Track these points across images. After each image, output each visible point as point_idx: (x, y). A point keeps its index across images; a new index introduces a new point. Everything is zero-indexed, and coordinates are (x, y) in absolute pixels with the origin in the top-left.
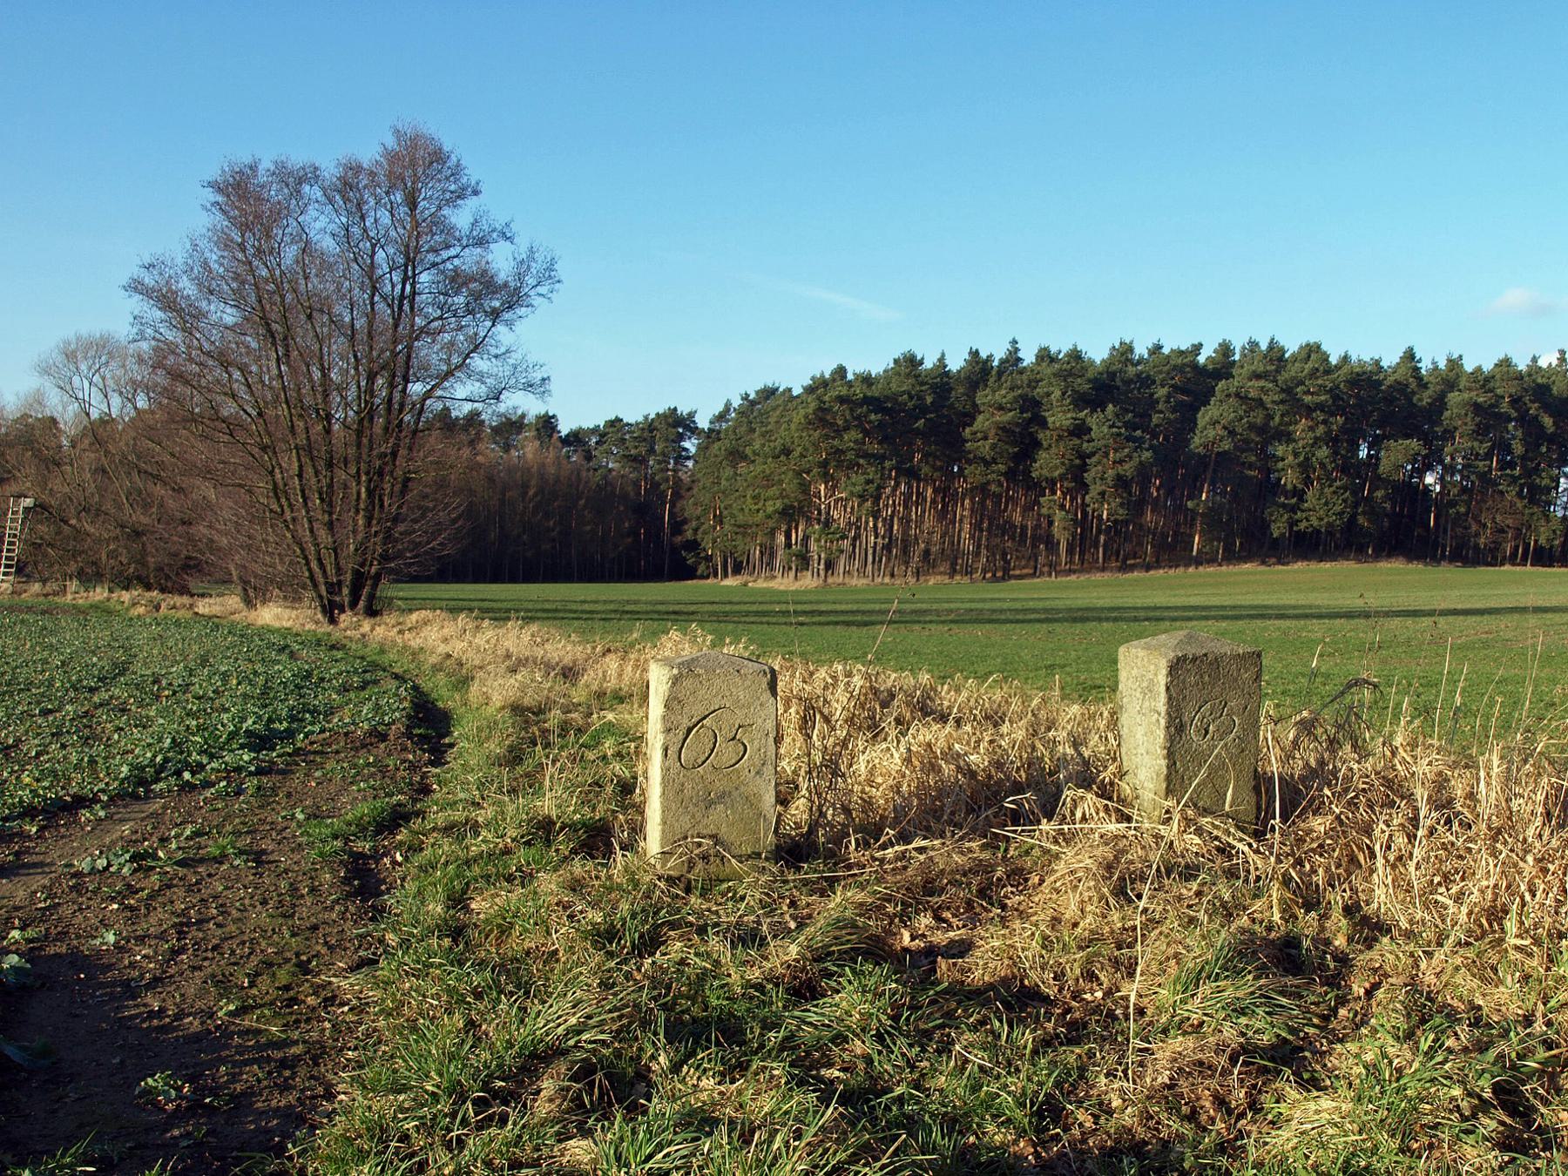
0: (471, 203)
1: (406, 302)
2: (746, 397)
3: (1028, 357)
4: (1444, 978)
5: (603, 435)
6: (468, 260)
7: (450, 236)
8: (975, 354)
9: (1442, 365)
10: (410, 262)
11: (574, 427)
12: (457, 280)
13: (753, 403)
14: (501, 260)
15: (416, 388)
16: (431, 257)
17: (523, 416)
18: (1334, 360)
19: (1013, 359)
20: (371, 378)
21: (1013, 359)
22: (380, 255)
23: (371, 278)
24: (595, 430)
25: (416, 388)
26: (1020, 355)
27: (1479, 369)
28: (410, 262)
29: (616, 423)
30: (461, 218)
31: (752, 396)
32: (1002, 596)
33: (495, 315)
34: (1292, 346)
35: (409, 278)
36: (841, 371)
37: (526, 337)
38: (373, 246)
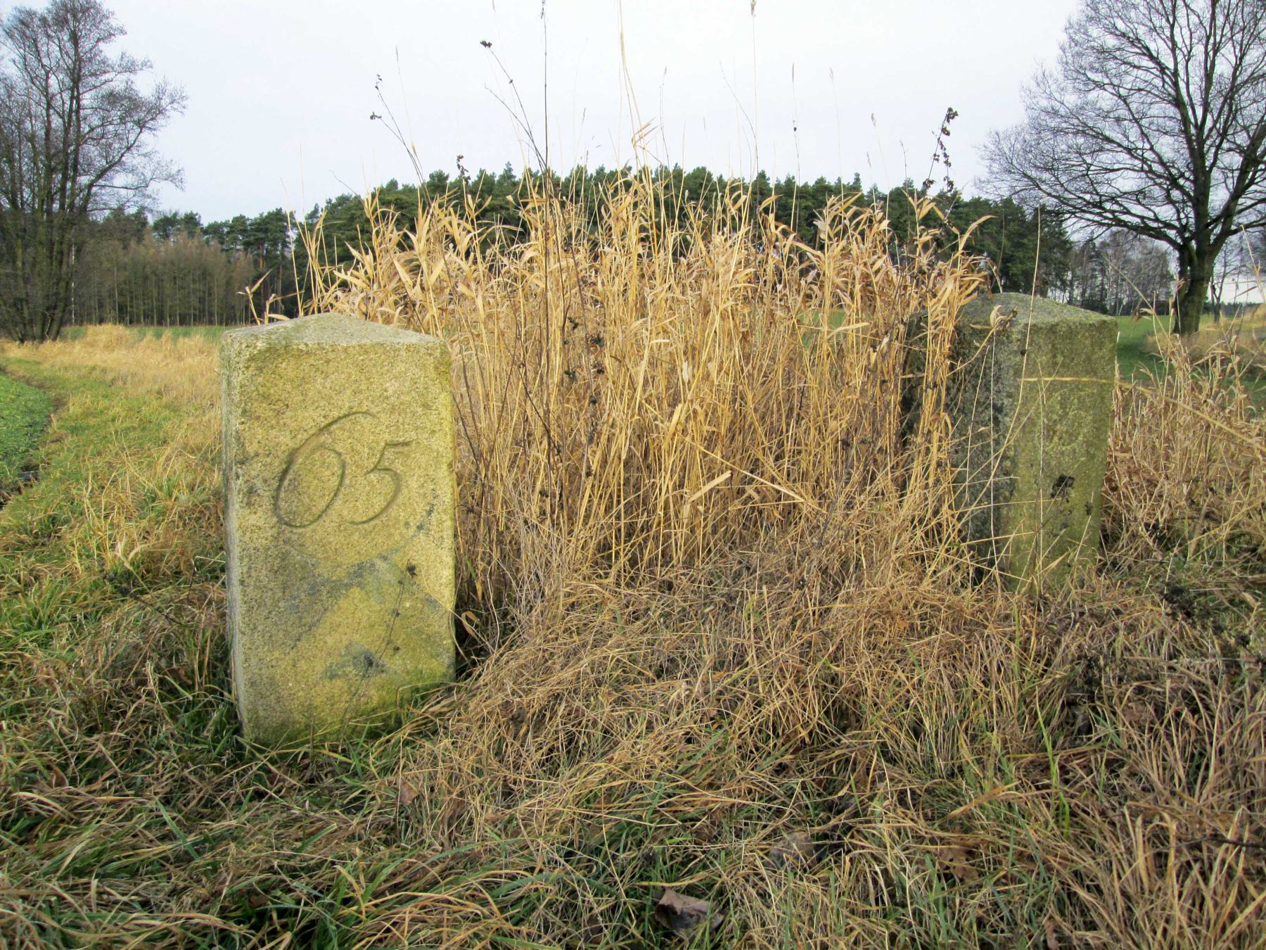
0: (119, 39)
1: (73, 116)
2: (329, 202)
3: (518, 175)
4: (748, 322)
5: (231, 227)
6: (117, 83)
7: (105, 67)
8: (482, 172)
9: (783, 182)
10: (76, 78)
11: (212, 221)
12: (112, 98)
13: (334, 206)
14: (144, 87)
15: (84, 180)
16: (92, 80)
17: (175, 215)
18: (715, 179)
19: (508, 176)
20: (51, 171)
21: (508, 176)
22: (53, 81)
23: (46, 96)
24: (225, 224)
25: (84, 180)
26: (513, 173)
27: (806, 186)
28: (76, 78)
29: (240, 220)
30: (110, 51)
31: (334, 201)
32: (583, 509)
33: (141, 125)
34: (688, 169)
35: (76, 98)
36: (393, 184)
37: (161, 143)
38: (47, 73)
